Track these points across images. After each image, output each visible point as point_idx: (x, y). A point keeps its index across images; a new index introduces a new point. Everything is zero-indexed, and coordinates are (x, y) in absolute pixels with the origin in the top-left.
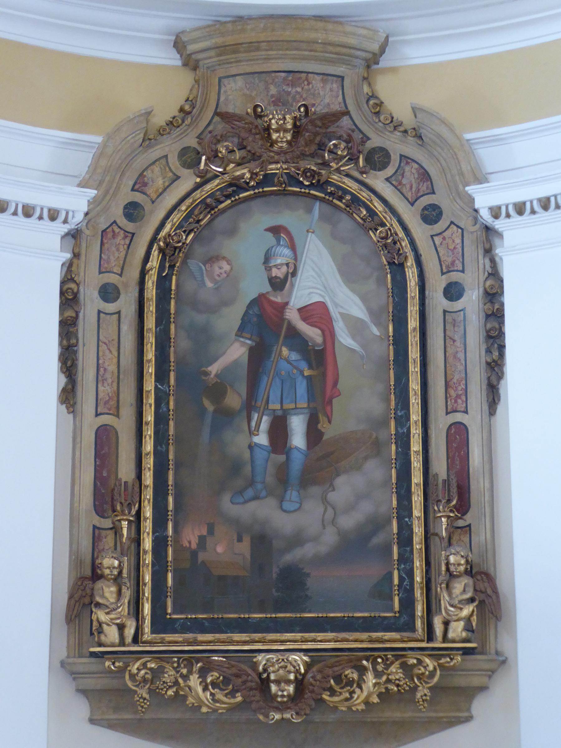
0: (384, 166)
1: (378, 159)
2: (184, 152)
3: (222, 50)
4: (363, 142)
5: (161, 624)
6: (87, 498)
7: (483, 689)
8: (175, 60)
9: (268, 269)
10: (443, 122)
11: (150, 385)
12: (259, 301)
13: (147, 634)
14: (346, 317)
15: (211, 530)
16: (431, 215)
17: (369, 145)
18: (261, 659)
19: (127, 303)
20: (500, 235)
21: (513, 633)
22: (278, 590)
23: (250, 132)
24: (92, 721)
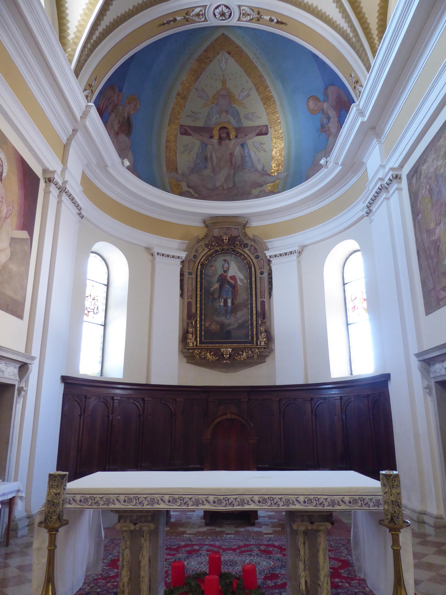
0: (247, 247)
1: (246, 246)
2: (205, 244)
3: (213, 223)
4: (243, 242)
5: (201, 342)
6: (185, 316)
7: (268, 356)
8: (202, 225)
9: (223, 269)
10: (259, 238)
11: (199, 293)
12: (221, 275)
13: (198, 345)
14: (239, 278)
15: (211, 323)
16: (257, 257)
17: (244, 243)
18: (222, 350)
19: (194, 276)
20: (271, 262)
21: (274, 344)
22: (225, 335)
23: (219, 240)
24: (187, 362)
